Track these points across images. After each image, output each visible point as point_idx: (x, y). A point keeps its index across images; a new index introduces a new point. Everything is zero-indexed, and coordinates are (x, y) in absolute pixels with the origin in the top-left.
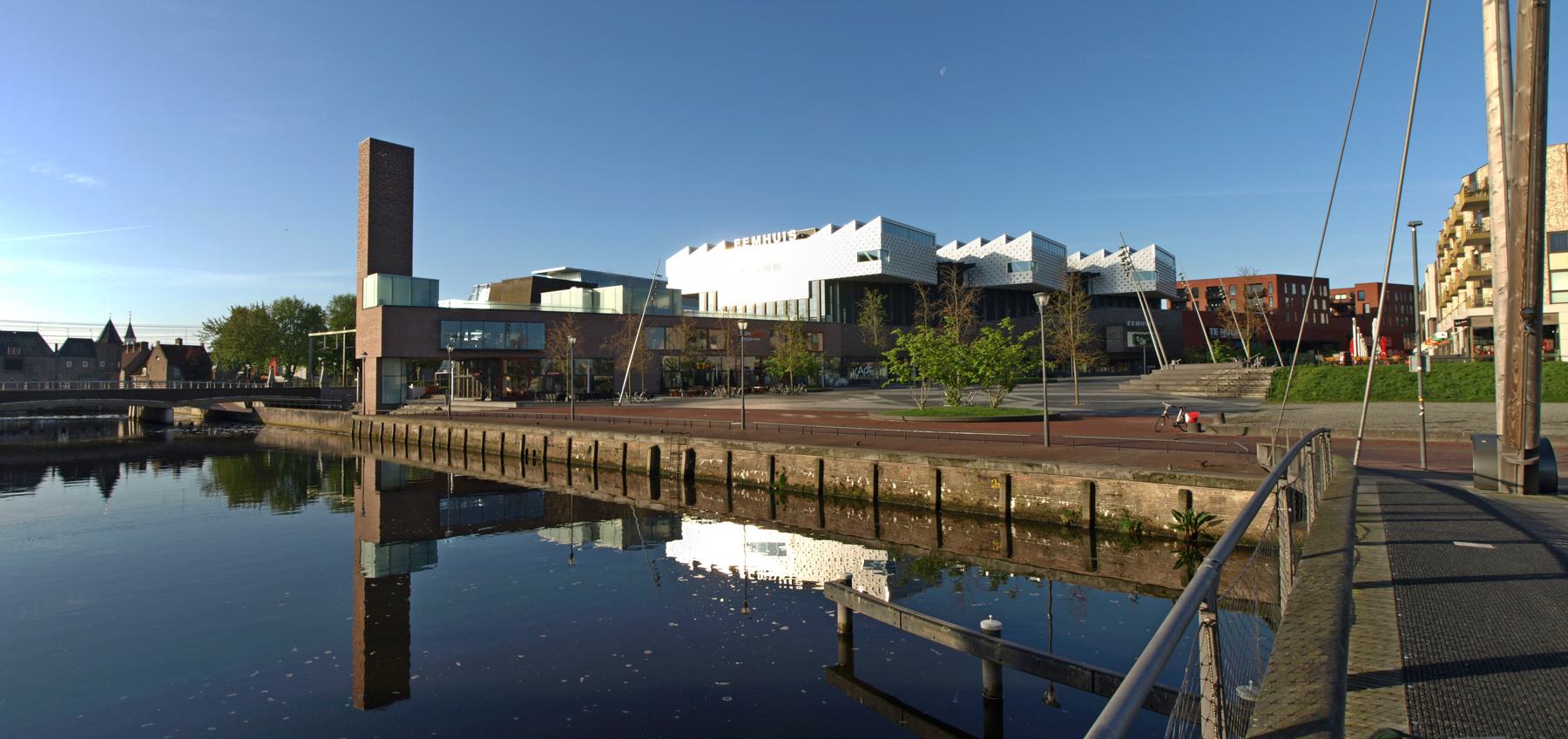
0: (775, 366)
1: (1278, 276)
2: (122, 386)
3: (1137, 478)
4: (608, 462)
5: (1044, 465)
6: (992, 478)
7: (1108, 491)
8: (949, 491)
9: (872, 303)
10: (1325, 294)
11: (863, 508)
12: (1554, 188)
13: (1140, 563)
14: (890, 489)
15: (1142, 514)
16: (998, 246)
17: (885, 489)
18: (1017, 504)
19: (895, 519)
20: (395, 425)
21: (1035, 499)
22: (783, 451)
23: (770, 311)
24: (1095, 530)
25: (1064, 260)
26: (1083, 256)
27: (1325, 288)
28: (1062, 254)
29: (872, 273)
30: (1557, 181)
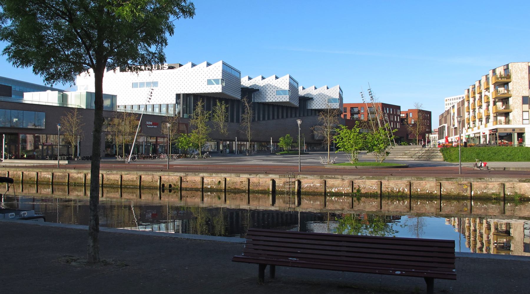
0: (182, 142)
1: (382, 104)
2: (482, 142)
3: (520, 181)
4: (235, 188)
5: (485, 178)
6: (464, 184)
7: (509, 186)
8: (445, 190)
9: (221, 109)
10: (399, 114)
11: (403, 200)
12: (524, 79)
13: (520, 209)
14: (417, 191)
15: (521, 193)
16: (270, 80)
17: (414, 191)
18: (474, 193)
19: (419, 203)
20: (23, 173)
21: (481, 191)
22: (359, 179)
23: (164, 109)
24: (505, 199)
25: (239, 80)
26: (250, 79)
27: (399, 110)
28: (238, 76)
29: (212, 92)
30: (525, 77)
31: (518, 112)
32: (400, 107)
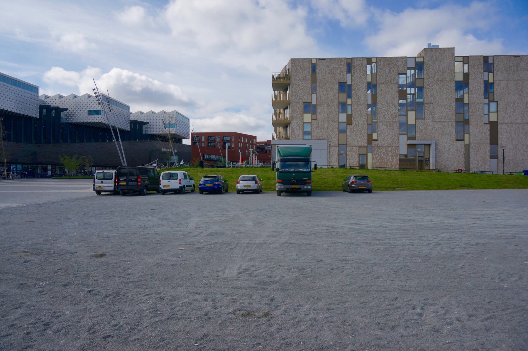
30: (307, 77)
31: (297, 123)
32: (256, 137)
